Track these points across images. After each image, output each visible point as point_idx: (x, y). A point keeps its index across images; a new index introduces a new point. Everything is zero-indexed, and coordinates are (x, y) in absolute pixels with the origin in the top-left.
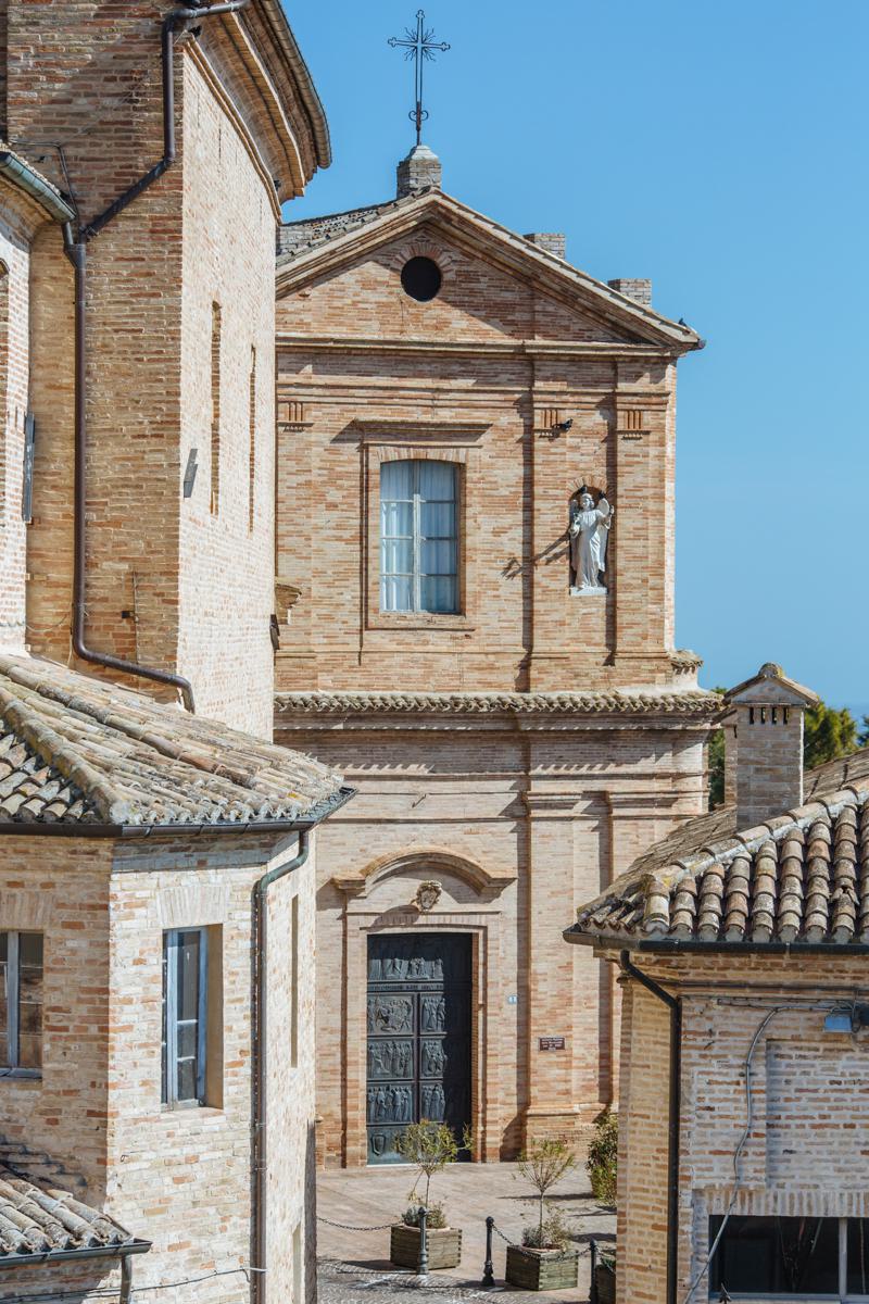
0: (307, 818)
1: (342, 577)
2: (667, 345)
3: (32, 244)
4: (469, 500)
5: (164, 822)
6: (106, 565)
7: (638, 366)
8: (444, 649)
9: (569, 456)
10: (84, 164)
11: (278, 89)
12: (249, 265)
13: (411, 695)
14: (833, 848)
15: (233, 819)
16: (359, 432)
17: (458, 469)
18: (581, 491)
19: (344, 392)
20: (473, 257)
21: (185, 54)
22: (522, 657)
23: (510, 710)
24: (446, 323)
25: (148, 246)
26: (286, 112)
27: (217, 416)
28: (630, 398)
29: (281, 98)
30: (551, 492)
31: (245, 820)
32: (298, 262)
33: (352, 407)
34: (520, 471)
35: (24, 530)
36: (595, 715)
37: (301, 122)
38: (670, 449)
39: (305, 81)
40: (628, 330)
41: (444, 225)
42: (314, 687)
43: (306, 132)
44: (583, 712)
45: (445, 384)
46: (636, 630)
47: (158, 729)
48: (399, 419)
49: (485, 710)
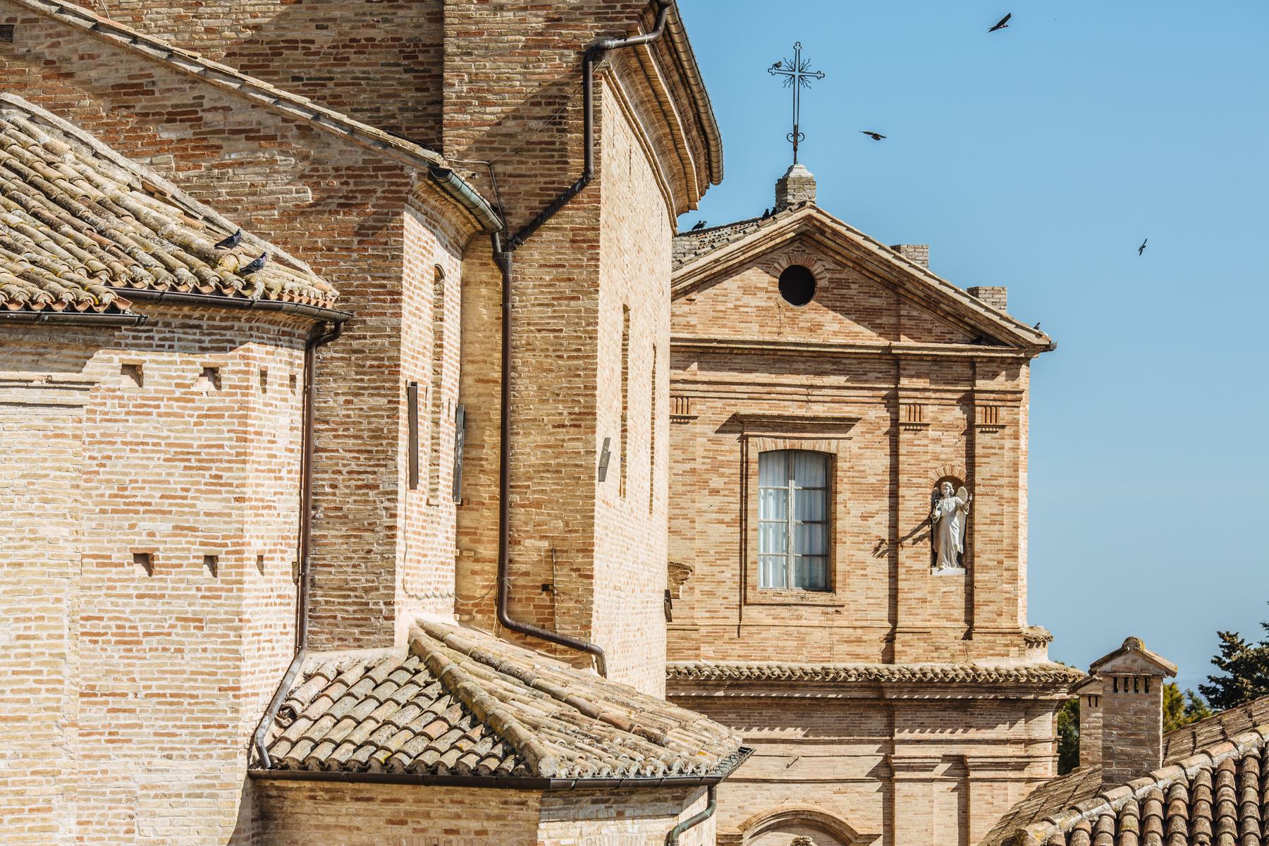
0: (712, 774)
1: (723, 556)
2: (1021, 347)
3: (464, 251)
4: (839, 487)
5: (587, 776)
6: (528, 542)
7: (993, 367)
8: (816, 623)
9: (931, 448)
10: (512, 179)
11: (680, 113)
12: (652, 272)
13: (785, 666)
14: (1191, 807)
15: (649, 774)
16: (738, 424)
17: (829, 460)
18: (938, 484)
19: (721, 388)
20: (844, 266)
21: (603, 81)
22: (888, 631)
23: (876, 680)
24: (820, 325)
25: (568, 255)
26: (686, 134)
27: (625, 408)
28: (986, 395)
29: (682, 121)
30: (915, 480)
31: (660, 775)
32: (685, 269)
33: (733, 402)
34: (887, 461)
35: (454, 510)
36: (954, 685)
37: (699, 143)
38: (1023, 442)
39: (705, 106)
40: (982, 334)
41: (818, 236)
42: (697, 656)
43: (702, 151)
44: (944, 682)
45: (818, 381)
46: (992, 607)
47: (577, 692)
48: (776, 413)
49: (853, 679)
